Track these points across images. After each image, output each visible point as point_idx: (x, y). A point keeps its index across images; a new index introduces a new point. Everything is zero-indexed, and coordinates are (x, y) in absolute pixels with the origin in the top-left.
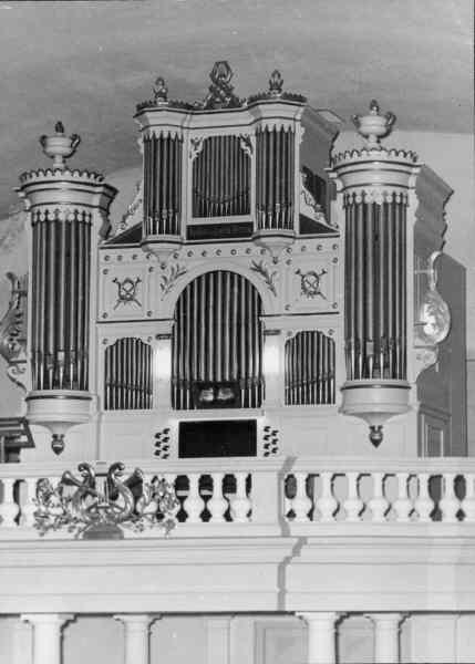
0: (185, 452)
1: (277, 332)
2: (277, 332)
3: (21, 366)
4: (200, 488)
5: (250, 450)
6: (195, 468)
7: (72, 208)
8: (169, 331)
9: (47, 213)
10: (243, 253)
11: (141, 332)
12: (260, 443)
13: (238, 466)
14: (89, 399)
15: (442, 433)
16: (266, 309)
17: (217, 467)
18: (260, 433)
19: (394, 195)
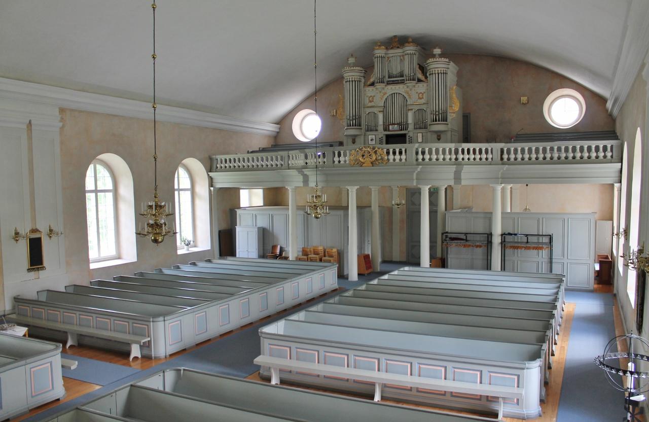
0: (387, 143)
1: (412, 110)
2: (412, 110)
3: (344, 120)
4: (550, 150)
5: (405, 142)
6: (391, 147)
7: (351, 77)
8: (382, 110)
9: (435, 71)
10: (422, 86)
11: (375, 110)
12: (407, 140)
13: (403, 147)
14: (362, 129)
15: (639, 129)
16: (409, 103)
17: (398, 147)
18: (407, 137)
19: (355, 78)
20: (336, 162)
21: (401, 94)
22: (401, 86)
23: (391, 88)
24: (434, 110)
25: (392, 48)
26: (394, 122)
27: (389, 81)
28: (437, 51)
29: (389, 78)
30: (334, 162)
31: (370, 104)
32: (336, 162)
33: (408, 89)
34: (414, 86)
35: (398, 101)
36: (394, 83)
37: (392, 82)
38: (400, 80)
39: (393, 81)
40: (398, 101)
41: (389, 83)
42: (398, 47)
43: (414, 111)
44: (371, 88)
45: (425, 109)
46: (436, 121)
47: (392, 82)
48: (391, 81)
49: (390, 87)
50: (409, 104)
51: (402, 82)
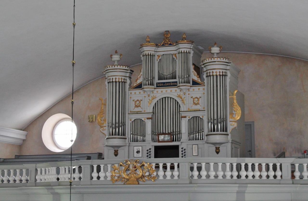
2: (185, 117)
8: (151, 117)
16: (182, 109)
20: (95, 179)
21: (173, 99)
22: (173, 89)
23: (162, 92)
24: (212, 118)
25: (163, 45)
26: (164, 132)
27: (159, 83)
28: (215, 50)
29: (159, 79)
30: (92, 178)
31: (137, 109)
32: (95, 179)
33: (182, 93)
34: (189, 90)
35: (169, 107)
36: (164, 85)
37: (162, 84)
38: (173, 82)
39: (164, 83)
40: (169, 107)
41: (159, 85)
42: (170, 44)
43: (187, 119)
44: (138, 91)
45: (201, 117)
46: (214, 131)
47: (162, 84)
48: (161, 83)
49: (160, 90)
50: (182, 110)
51: (174, 85)
